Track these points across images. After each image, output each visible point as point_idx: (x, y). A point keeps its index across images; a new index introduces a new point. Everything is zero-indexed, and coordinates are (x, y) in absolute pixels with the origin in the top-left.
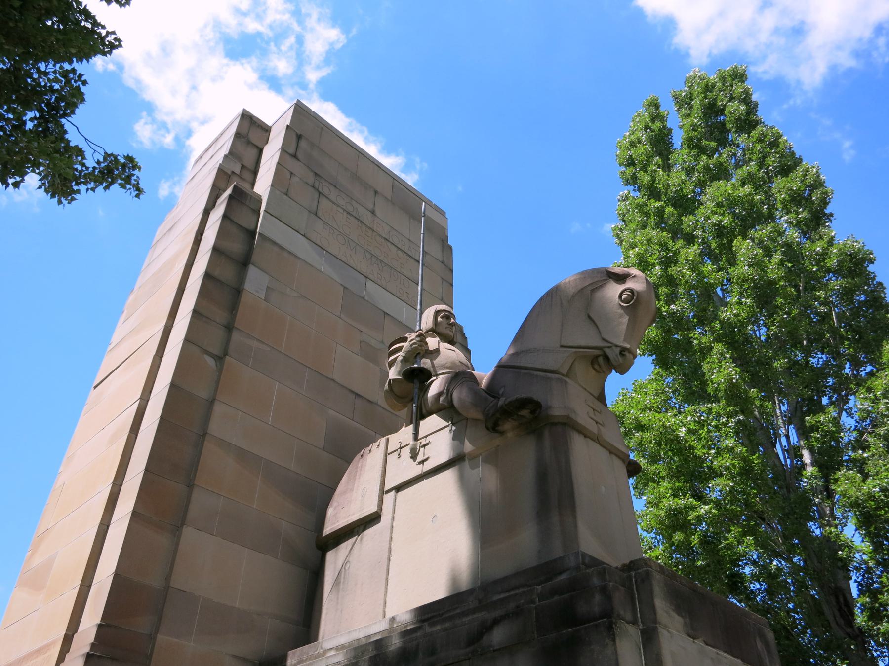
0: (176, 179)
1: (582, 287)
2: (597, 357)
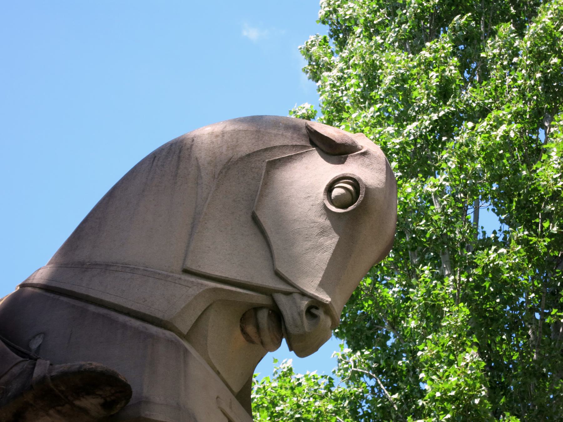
0: (212, 146)
1: (248, 152)
2: (256, 309)
